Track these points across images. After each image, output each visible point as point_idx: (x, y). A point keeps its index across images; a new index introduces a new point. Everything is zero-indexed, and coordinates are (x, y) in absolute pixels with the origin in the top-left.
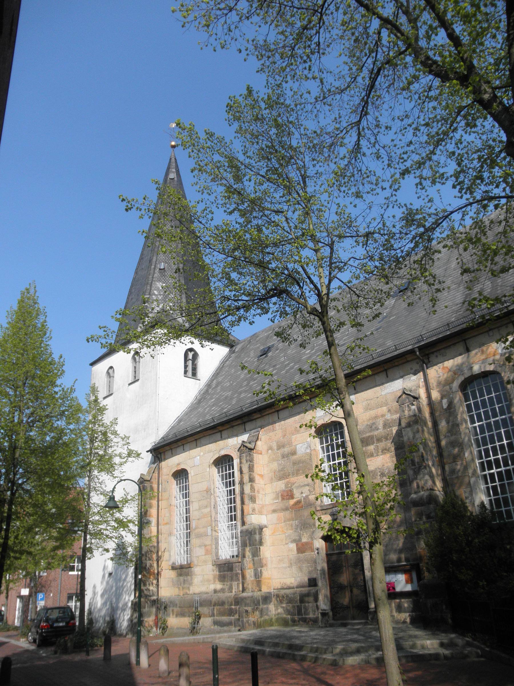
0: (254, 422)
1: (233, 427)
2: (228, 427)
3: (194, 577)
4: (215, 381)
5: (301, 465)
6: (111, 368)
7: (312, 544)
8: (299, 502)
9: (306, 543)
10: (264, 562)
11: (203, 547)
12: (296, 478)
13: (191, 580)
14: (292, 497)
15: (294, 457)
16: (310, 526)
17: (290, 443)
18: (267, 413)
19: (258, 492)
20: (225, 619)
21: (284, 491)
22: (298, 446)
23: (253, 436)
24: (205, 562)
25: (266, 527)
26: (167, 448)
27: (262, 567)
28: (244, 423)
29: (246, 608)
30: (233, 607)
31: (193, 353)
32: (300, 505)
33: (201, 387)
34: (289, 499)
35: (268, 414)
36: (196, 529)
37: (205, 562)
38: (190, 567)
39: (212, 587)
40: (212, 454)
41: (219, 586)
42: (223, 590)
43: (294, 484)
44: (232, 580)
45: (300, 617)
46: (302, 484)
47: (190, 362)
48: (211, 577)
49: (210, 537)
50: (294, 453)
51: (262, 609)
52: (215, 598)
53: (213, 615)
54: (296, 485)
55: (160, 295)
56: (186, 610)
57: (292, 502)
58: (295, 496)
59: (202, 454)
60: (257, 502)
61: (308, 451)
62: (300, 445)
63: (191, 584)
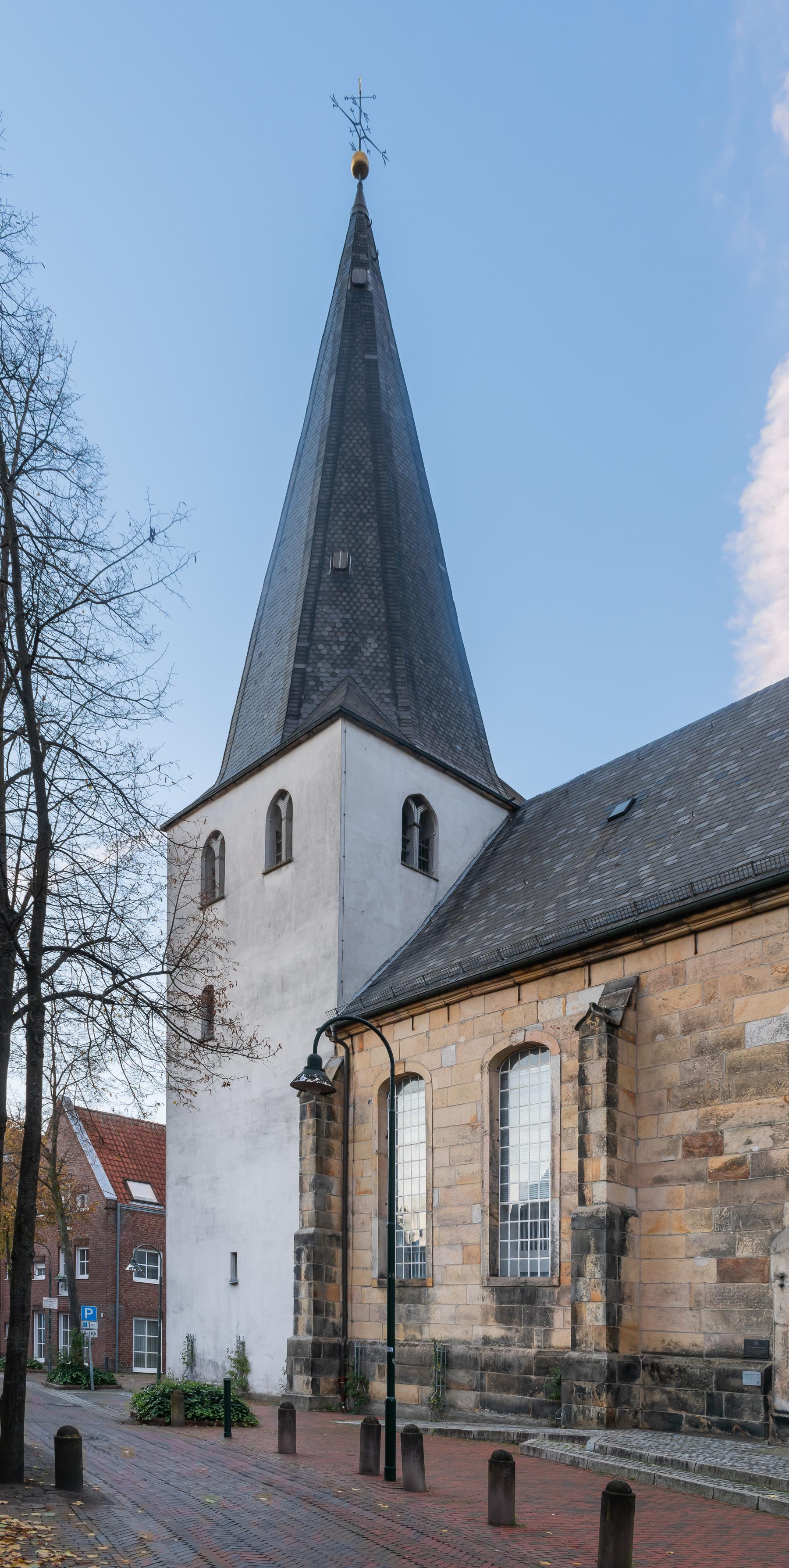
0: (618, 962)
1: (553, 973)
3: (432, 1307)
4: (476, 886)
5: (755, 1074)
7: (766, 1263)
8: (738, 1163)
9: (749, 1261)
10: (627, 1291)
11: (459, 1248)
12: (737, 1105)
13: (427, 1311)
14: (718, 1150)
15: (736, 1053)
16: (766, 1223)
17: (725, 1019)
19: (623, 1132)
20: (512, 1398)
21: (694, 1135)
22: (748, 1027)
23: (617, 997)
24: (462, 1278)
27: (622, 1301)
28: (589, 964)
29: (582, 1384)
30: (533, 1377)
31: (421, 809)
32: (741, 1171)
33: (440, 898)
34: (706, 1155)
36: (440, 1206)
37: (462, 1278)
38: (424, 1286)
39: (479, 1331)
40: (489, 1040)
41: (496, 1331)
42: (505, 1341)
43: (726, 1119)
44: (531, 1320)
45: (715, 1418)
46: (750, 1121)
47: (416, 831)
48: (477, 1312)
49: (479, 1227)
50: (736, 1043)
51: (619, 1390)
52: (487, 1353)
53: (480, 1388)
54: (731, 1121)
56: (414, 1371)
57: (715, 1162)
58: (727, 1149)
59: (462, 1039)
60: (619, 1156)
62: (759, 1023)
63: (426, 1321)
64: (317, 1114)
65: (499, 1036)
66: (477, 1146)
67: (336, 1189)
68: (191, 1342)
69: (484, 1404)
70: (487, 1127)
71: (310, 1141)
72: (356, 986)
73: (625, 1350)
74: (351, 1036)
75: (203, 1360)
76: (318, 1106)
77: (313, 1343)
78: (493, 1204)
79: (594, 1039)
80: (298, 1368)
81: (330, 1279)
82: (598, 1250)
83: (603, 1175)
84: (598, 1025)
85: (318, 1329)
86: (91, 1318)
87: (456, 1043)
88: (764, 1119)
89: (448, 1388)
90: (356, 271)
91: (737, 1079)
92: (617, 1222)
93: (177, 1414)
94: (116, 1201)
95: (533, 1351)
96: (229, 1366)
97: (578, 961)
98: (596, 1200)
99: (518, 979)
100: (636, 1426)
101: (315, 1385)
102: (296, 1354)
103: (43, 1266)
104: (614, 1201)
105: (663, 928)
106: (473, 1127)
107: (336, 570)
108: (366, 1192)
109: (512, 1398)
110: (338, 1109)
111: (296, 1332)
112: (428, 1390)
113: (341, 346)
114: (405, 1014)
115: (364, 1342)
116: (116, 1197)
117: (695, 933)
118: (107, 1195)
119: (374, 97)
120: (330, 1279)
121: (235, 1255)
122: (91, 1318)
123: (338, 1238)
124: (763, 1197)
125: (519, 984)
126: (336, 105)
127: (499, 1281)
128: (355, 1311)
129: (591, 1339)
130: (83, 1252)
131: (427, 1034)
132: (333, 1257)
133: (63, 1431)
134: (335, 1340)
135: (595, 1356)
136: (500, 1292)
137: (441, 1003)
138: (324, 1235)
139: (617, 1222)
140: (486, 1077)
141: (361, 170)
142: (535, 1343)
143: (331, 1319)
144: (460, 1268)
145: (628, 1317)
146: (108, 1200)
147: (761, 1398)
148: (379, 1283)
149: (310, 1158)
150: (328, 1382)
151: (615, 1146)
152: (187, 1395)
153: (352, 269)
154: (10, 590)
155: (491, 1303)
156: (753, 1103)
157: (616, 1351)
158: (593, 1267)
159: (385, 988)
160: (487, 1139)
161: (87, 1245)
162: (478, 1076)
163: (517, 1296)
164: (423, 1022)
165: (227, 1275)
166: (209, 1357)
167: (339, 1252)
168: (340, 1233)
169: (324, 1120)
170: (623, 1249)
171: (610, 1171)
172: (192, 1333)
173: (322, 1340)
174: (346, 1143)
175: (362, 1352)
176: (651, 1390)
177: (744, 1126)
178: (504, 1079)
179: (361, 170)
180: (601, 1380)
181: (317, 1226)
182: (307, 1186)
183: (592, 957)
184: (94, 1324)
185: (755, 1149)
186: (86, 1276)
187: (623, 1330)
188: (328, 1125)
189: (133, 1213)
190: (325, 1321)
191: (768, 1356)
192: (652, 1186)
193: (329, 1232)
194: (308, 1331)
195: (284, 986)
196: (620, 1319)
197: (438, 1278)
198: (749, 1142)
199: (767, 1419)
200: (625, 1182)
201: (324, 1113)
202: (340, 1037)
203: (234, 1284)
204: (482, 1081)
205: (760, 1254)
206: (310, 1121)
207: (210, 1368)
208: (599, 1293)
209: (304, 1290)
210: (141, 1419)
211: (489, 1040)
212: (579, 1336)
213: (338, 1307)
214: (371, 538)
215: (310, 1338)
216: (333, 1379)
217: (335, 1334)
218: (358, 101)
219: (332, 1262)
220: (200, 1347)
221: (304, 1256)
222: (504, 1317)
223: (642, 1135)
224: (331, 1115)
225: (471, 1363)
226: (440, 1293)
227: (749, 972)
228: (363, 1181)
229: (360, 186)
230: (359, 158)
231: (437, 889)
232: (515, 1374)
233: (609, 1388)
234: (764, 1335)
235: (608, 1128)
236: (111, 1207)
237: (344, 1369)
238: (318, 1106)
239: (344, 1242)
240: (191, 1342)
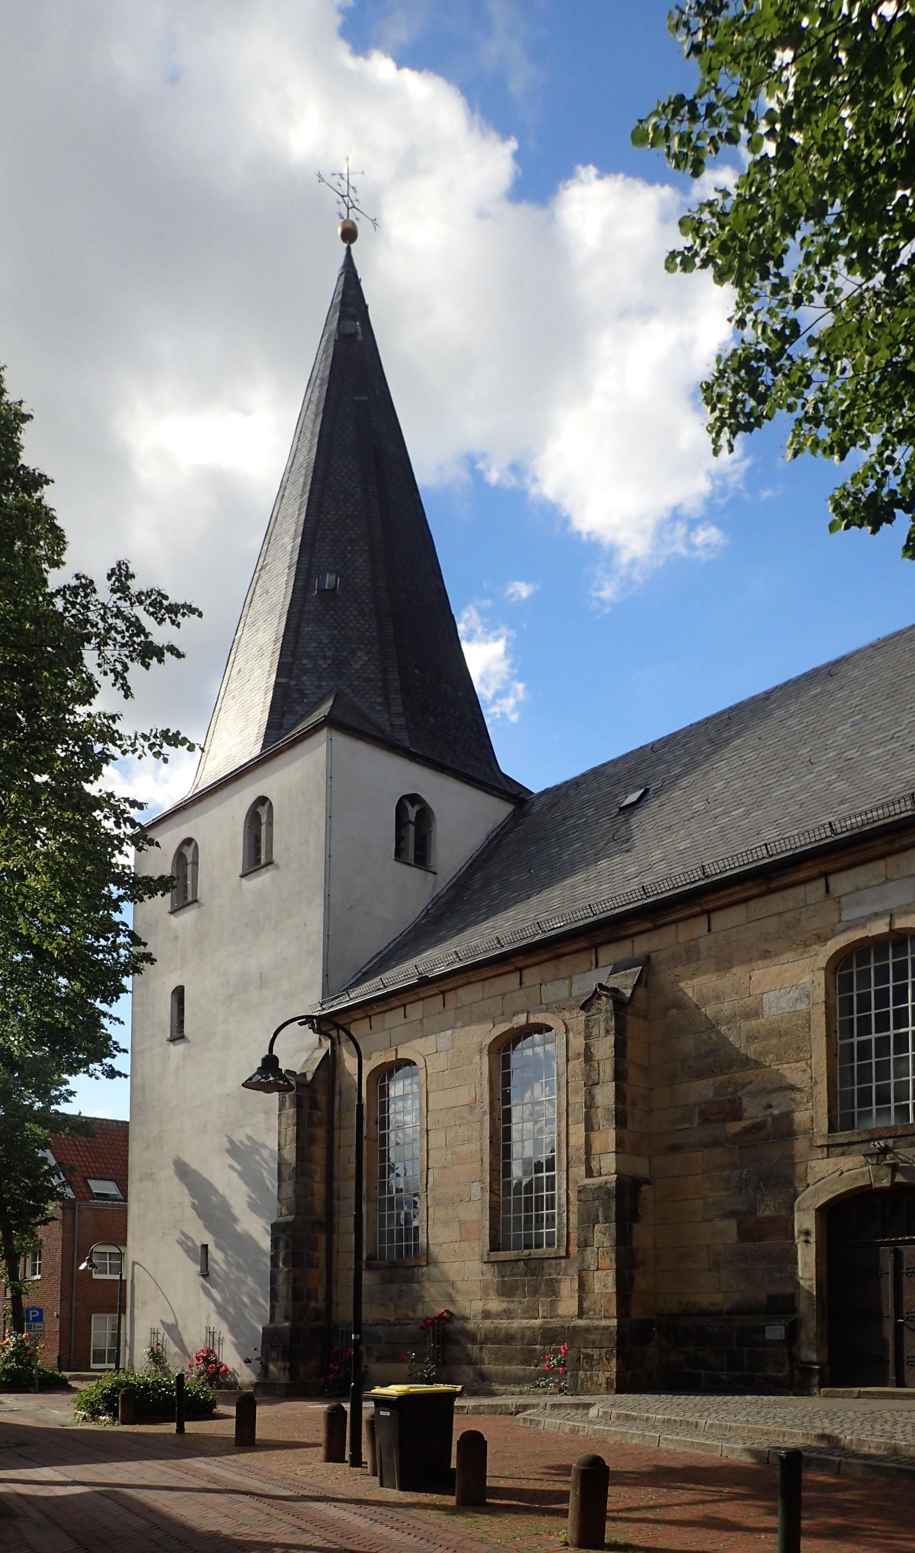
1: (558, 957)
2: (545, 957)
5: (774, 1041)
6: (188, 841)
9: (771, 1220)
14: (736, 1114)
18: (674, 917)
19: (633, 1104)
25: (647, 1182)
26: (359, 1014)
31: (417, 808)
33: (438, 890)
35: (676, 922)
41: (495, 1304)
42: (508, 1314)
43: (744, 1086)
44: (535, 1292)
47: (412, 828)
50: (756, 1013)
55: (325, 658)
57: (734, 1127)
58: (745, 1115)
60: (630, 1127)
61: (801, 1007)
82: (607, 1219)
94: (74, 1201)
110: (322, 1098)
114: (397, 1003)
131: (421, 1021)
135: (604, 1323)
140: (486, 1059)
143: (313, 1304)
151: (625, 1118)
160: (487, 1117)
162: (477, 1059)
167: (322, 1238)
168: (324, 1219)
181: (297, 1214)
198: (770, 1106)
213: (321, 1292)
224: (314, 1105)
229: (349, 250)
230: (349, 225)
235: (616, 1102)
239: (329, 1225)
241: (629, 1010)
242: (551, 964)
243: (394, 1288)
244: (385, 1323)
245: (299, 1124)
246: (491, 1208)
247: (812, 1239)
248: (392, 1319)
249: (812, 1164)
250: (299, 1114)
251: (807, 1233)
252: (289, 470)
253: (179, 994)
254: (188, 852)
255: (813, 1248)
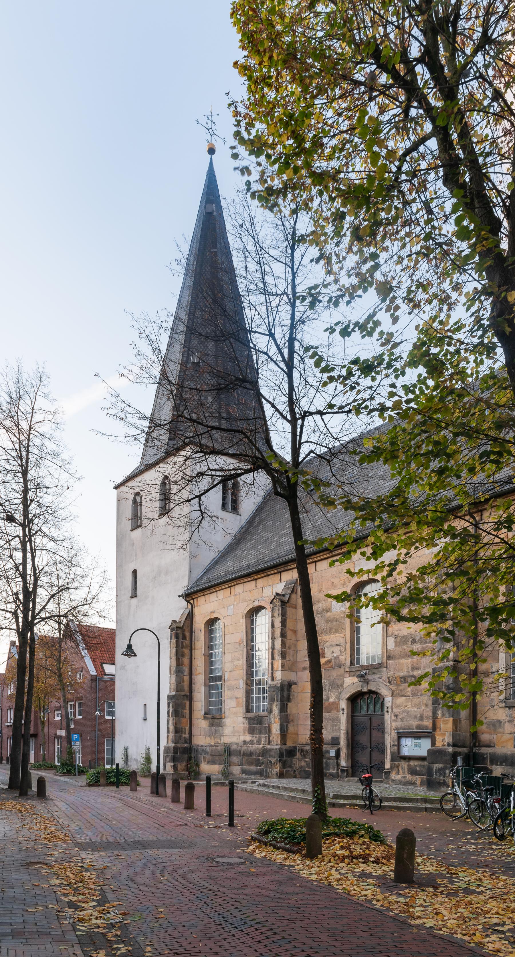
1: (268, 575)
2: (263, 575)
3: (225, 727)
5: (335, 623)
7: (338, 704)
9: (333, 703)
15: (329, 615)
19: (289, 648)
23: (288, 588)
24: (235, 713)
27: (288, 722)
28: (281, 572)
29: (271, 759)
32: (331, 665)
38: (221, 718)
39: (242, 738)
41: (248, 738)
42: (251, 742)
43: (326, 642)
48: (241, 730)
51: (285, 761)
53: (241, 764)
56: (217, 758)
59: (235, 603)
60: (288, 658)
63: (222, 735)
64: (177, 637)
65: (249, 602)
66: (241, 652)
67: (186, 673)
68: (126, 749)
69: (243, 772)
70: (245, 644)
71: (174, 650)
72: (198, 572)
73: (290, 744)
74: (193, 599)
75: (131, 759)
76: (177, 634)
77: (174, 747)
78: (248, 679)
79: (277, 608)
80: (168, 760)
81: (183, 716)
82: (277, 701)
83: (280, 668)
84: (278, 602)
85: (177, 741)
86: (76, 740)
87: (233, 605)
88: (338, 643)
89: (230, 765)
90: (208, 205)
91: (329, 625)
92: (286, 688)
93: (103, 781)
94: (96, 676)
95: (261, 746)
96: (143, 761)
97: (276, 571)
98: (278, 678)
99: (255, 577)
100: (295, 777)
101: (175, 768)
102: (167, 753)
103: (59, 712)
104: (285, 679)
105: (288, 568)
106: (240, 644)
107: (194, 363)
108: (200, 674)
109: (253, 768)
110: (187, 634)
111: (167, 742)
112: (222, 766)
113: (200, 246)
114: (213, 590)
115: (198, 746)
116: (96, 674)
117: (316, 562)
118: (92, 673)
119: (218, 115)
120: (183, 716)
121: (145, 705)
122: (76, 740)
123: (187, 696)
124: (337, 676)
125: (256, 579)
126: (198, 122)
127: (250, 715)
128: (195, 731)
129: (275, 740)
130: (80, 704)
131: (222, 599)
132: (185, 705)
133: (39, 778)
134: (185, 745)
135: (276, 747)
136: (250, 719)
137: (227, 586)
138: (180, 695)
139: (286, 688)
140: (244, 621)
141: (212, 151)
142: (262, 743)
143: (184, 735)
144: (234, 709)
145: (291, 729)
146: (92, 675)
147: (336, 761)
148: (204, 717)
149: (174, 658)
150: (181, 766)
151: (286, 655)
152: (108, 773)
153: (206, 204)
154: (28, 543)
155: (246, 725)
156: (334, 636)
157: (285, 744)
158: (276, 709)
159: (209, 576)
160: (245, 649)
161: (81, 700)
162: (241, 620)
163: (256, 722)
164: (221, 594)
165: (142, 715)
166: (134, 757)
167: (188, 703)
168: (188, 694)
169: (181, 640)
170: (289, 699)
171: (283, 666)
172: (127, 745)
173: (179, 745)
174: (191, 650)
175: (197, 750)
176: (301, 761)
177: (331, 646)
178: (253, 622)
179: (212, 151)
180: (277, 757)
181: (177, 691)
182: (173, 672)
183: (280, 570)
184: (78, 743)
185: (335, 655)
186: (81, 717)
187: (289, 735)
188: (182, 642)
189: (105, 681)
190: (181, 736)
191: (339, 744)
192: (302, 671)
193: (183, 693)
194: (173, 742)
195: (167, 572)
196: (287, 730)
197: (227, 714)
198: (333, 653)
199: (338, 770)
200: (291, 669)
201: (181, 637)
202: (188, 599)
203: (145, 720)
204: (242, 622)
205: (337, 700)
206: (174, 641)
207: (135, 762)
208: (277, 719)
209: (171, 722)
210: (90, 785)
211: (245, 604)
212: (271, 738)
213: (187, 729)
214: (211, 345)
215: (173, 745)
216: (184, 764)
217: (186, 742)
218: (210, 117)
219: (184, 707)
220: (130, 752)
221: (171, 705)
222: (251, 731)
223: (299, 649)
224: (184, 637)
225: (239, 753)
226: (227, 721)
227: (333, 580)
228: (198, 668)
229: (211, 159)
230: (211, 146)
231: (241, 519)
232: (254, 757)
233: (280, 760)
234: (338, 735)
235: (282, 647)
236: (94, 679)
237: (190, 758)
238: (177, 634)
239: (190, 698)
240: (126, 749)
241: (288, 604)
242: (266, 578)
243: (213, 728)
244: (210, 745)
245: (177, 647)
246: (246, 692)
247: (345, 712)
248: (213, 744)
249: (345, 679)
250: (177, 642)
251: (343, 710)
252: (183, 287)
253: (135, 572)
254: (138, 498)
255: (345, 715)
